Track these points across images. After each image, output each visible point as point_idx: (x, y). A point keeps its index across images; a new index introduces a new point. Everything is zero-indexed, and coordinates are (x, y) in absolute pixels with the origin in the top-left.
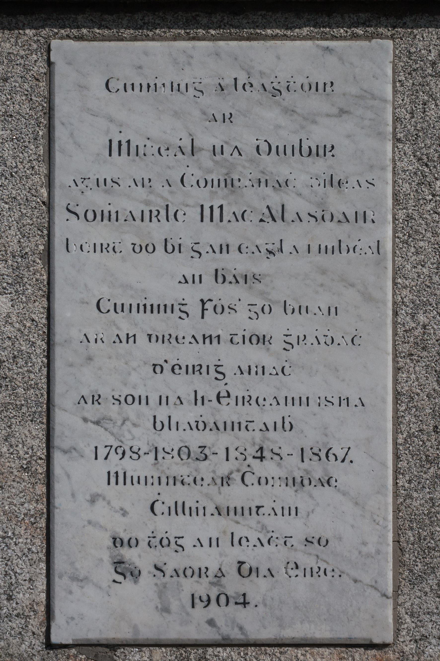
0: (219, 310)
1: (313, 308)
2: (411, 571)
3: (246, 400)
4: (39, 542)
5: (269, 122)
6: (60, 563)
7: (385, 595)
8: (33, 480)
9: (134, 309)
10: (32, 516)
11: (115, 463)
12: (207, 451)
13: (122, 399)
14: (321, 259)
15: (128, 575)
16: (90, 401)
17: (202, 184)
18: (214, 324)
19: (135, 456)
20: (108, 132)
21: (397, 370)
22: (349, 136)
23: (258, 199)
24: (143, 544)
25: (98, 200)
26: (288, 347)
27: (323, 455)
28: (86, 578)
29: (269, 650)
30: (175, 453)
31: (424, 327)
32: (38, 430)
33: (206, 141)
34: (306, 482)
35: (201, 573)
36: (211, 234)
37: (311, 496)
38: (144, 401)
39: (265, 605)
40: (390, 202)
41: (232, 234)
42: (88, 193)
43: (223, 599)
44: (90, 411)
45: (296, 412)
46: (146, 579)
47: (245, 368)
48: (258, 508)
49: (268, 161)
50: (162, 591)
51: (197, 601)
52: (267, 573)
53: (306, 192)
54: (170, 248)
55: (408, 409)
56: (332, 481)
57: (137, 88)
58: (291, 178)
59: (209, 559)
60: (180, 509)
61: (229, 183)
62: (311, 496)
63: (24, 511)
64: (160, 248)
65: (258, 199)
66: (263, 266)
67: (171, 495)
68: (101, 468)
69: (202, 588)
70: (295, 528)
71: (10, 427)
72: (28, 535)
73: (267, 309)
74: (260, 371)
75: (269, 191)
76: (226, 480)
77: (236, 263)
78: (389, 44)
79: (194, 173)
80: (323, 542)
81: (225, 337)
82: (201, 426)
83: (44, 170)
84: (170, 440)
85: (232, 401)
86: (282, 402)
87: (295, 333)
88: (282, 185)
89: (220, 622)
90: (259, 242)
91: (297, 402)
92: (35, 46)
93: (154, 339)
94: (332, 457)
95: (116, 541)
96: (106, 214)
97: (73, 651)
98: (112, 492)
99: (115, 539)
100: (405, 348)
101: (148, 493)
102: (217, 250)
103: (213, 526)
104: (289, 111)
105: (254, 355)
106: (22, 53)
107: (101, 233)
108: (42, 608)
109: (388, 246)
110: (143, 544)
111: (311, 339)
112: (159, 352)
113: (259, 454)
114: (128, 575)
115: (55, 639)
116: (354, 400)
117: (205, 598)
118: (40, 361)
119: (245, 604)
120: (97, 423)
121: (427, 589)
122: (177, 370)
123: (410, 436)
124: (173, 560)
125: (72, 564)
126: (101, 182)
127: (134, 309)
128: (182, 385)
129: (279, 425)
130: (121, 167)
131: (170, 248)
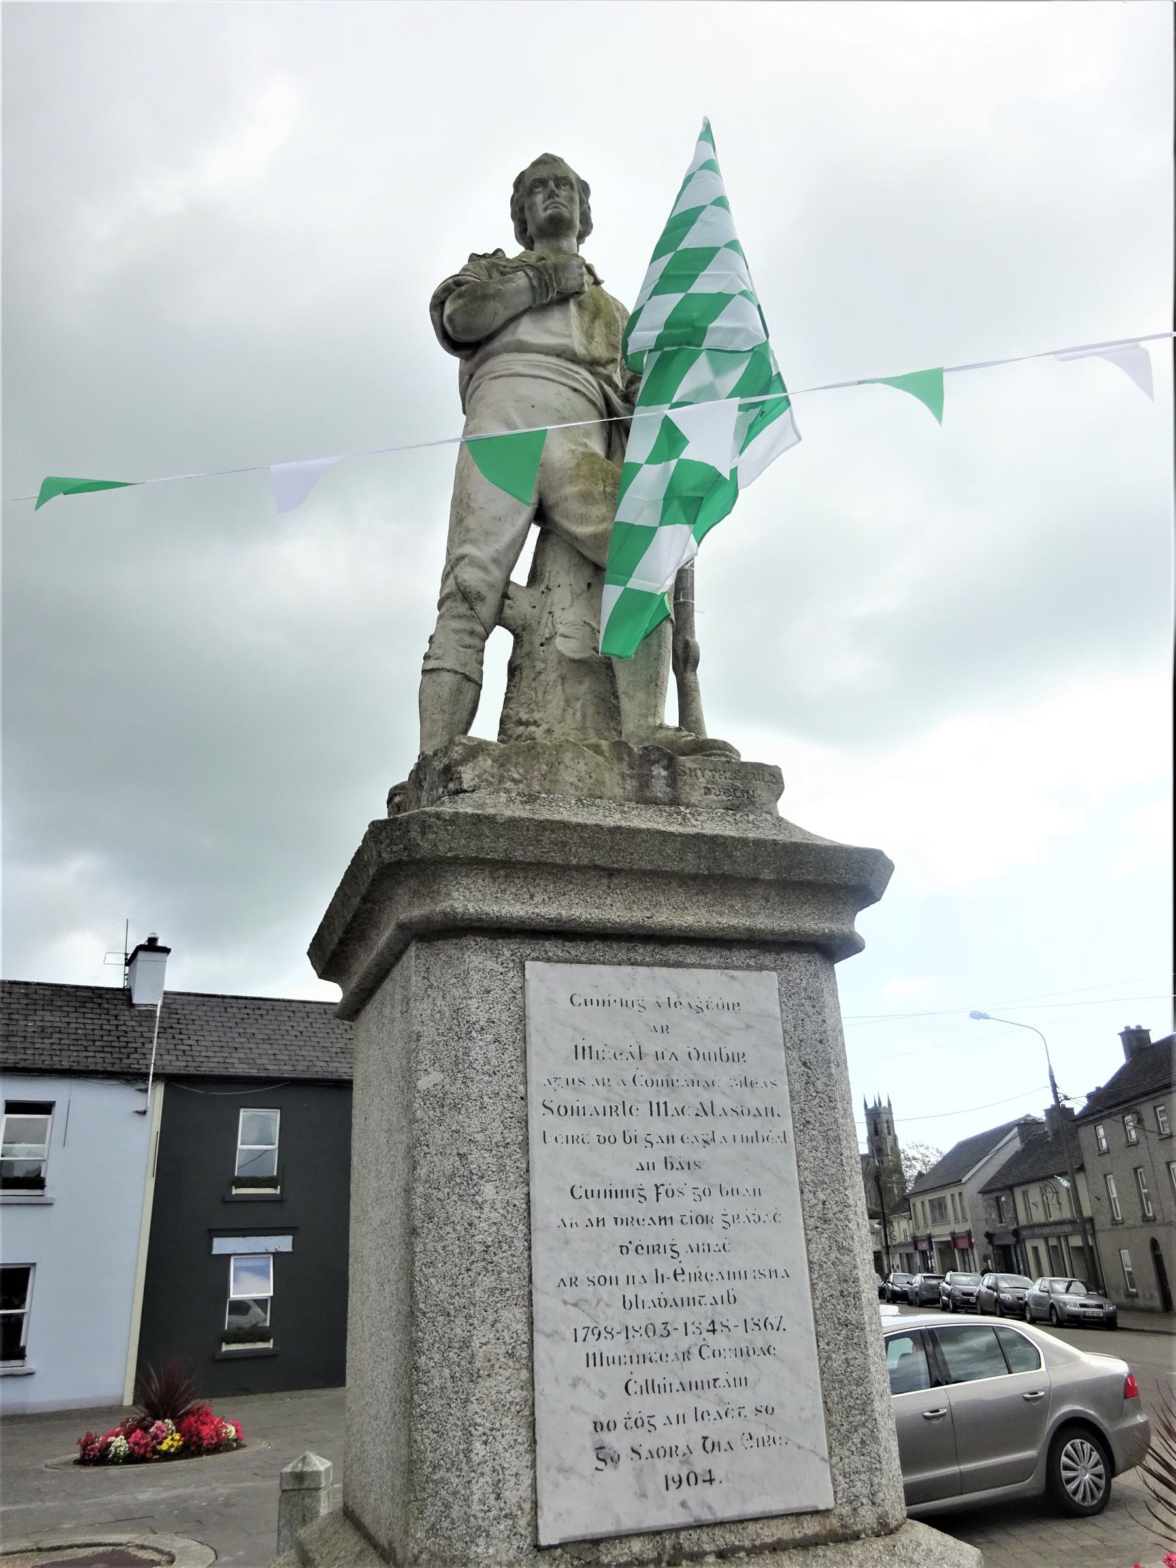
0: (670, 1193)
1: (742, 1191)
2: (839, 1431)
3: (697, 1277)
4: (523, 1435)
5: (689, 1033)
6: (544, 1451)
7: (823, 1459)
8: (518, 1366)
9: (602, 1194)
10: (517, 1404)
11: (593, 1345)
12: (669, 1327)
13: (596, 1281)
14: (740, 1146)
15: (609, 1460)
16: (568, 1284)
17: (650, 1083)
18: (666, 1206)
19: (609, 1336)
20: (573, 1039)
21: (808, 1241)
22: (754, 1046)
23: (691, 1097)
24: (620, 1426)
25: (568, 1097)
26: (726, 1225)
27: (762, 1324)
28: (571, 1468)
29: (733, 1528)
30: (643, 1331)
31: (824, 1203)
32: (520, 1313)
33: (650, 1048)
34: (751, 1352)
35: (671, 1452)
36: (659, 1127)
37: (756, 1365)
38: (614, 1282)
39: (728, 1480)
40: (788, 1099)
41: (677, 1125)
42: (559, 1090)
43: (692, 1477)
44: (570, 1293)
45: (737, 1285)
46: (625, 1463)
47: (695, 1247)
48: (715, 1380)
49: (697, 1065)
50: (639, 1474)
51: (670, 1482)
52: (727, 1447)
53: (728, 1090)
54: (628, 1140)
55: (820, 1276)
56: (771, 1350)
57: (595, 1003)
58: (716, 1079)
59: (675, 1436)
60: (650, 1387)
61: (671, 1083)
62: (756, 1365)
63: (510, 1399)
64: (620, 1139)
65: (691, 1097)
66: (701, 1154)
67: (641, 1373)
68: (581, 1349)
69: (673, 1467)
70: (744, 1398)
71: (496, 1312)
72: (514, 1425)
73: (707, 1192)
74: (706, 1248)
75: (700, 1090)
76: (686, 1355)
77: (679, 1151)
78: (774, 974)
79: (643, 1075)
80: (770, 1411)
81: (677, 1218)
82: (663, 1303)
83: (521, 1070)
84: (636, 1318)
85: (686, 1277)
86: (726, 1276)
87: (730, 1212)
88: (710, 1085)
89: (691, 1503)
90: (696, 1133)
91: (737, 1276)
92: (511, 965)
93: (619, 1222)
94: (769, 1327)
95: (598, 1426)
96: (575, 1110)
97: (559, 1551)
98: (591, 1374)
99: (595, 1423)
100: (812, 1222)
101: (620, 1373)
102: (665, 1140)
103: (685, 1402)
104: (709, 1025)
105: (700, 1234)
106: (501, 970)
107: (571, 1126)
108: (527, 1506)
109: (791, 1136)
110: (620, 1426)
111: (743, 1218)
112: (623, 1234)
113: (711, 1328)
114: (609, 1460)
115: (544, 1541)
116: (781, 1273)
117: (677, 1479)
118: (520, 1244)
119: (711, 1481)
120: (575, 1305)
121: (854, 1449)
122: (640, 1251)
123: (824, 1300)
124: (648, 1442)
125: (558, 1453)
126: (570, 1081)
127: (602, 1194)
128: (642, 1265)
129: (725, 1299)
130: (587, 1069)
131: (628, 1140)
